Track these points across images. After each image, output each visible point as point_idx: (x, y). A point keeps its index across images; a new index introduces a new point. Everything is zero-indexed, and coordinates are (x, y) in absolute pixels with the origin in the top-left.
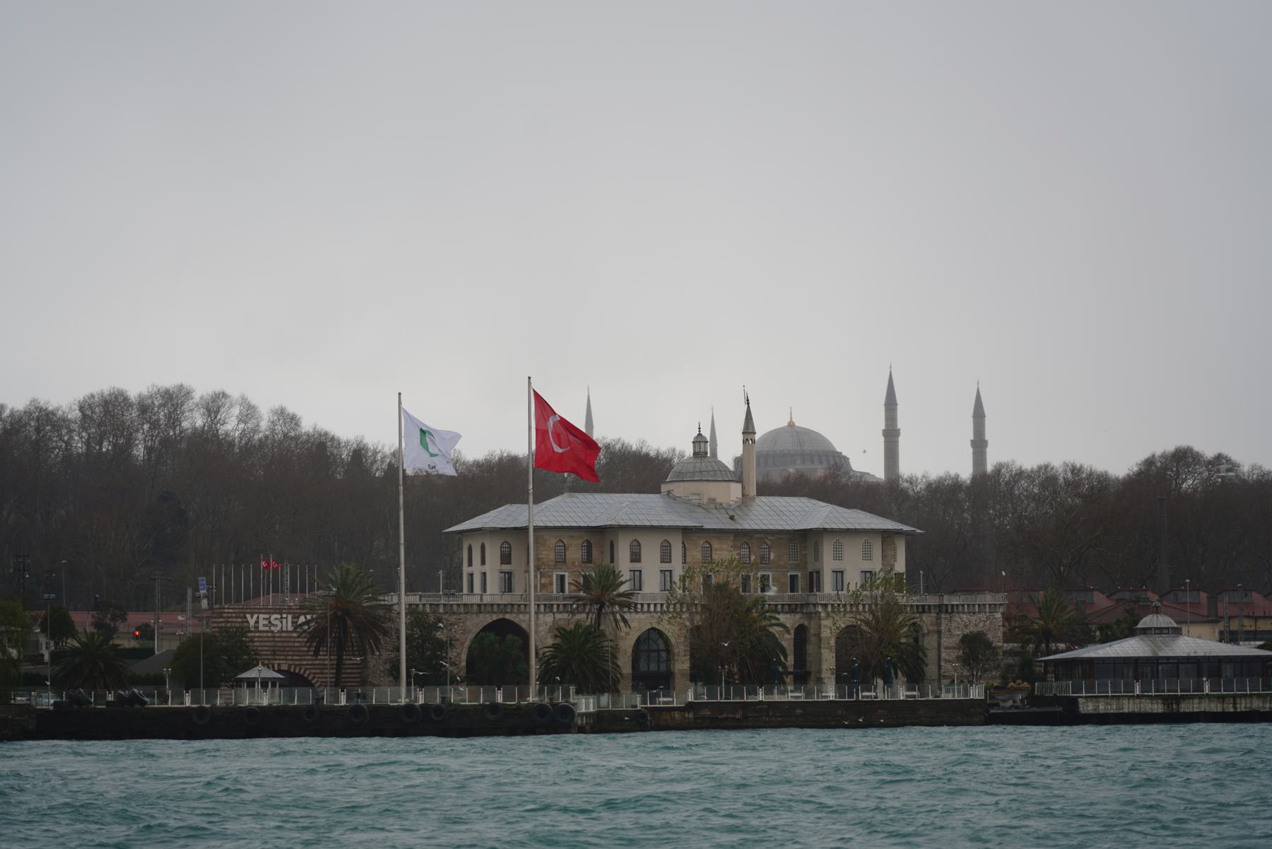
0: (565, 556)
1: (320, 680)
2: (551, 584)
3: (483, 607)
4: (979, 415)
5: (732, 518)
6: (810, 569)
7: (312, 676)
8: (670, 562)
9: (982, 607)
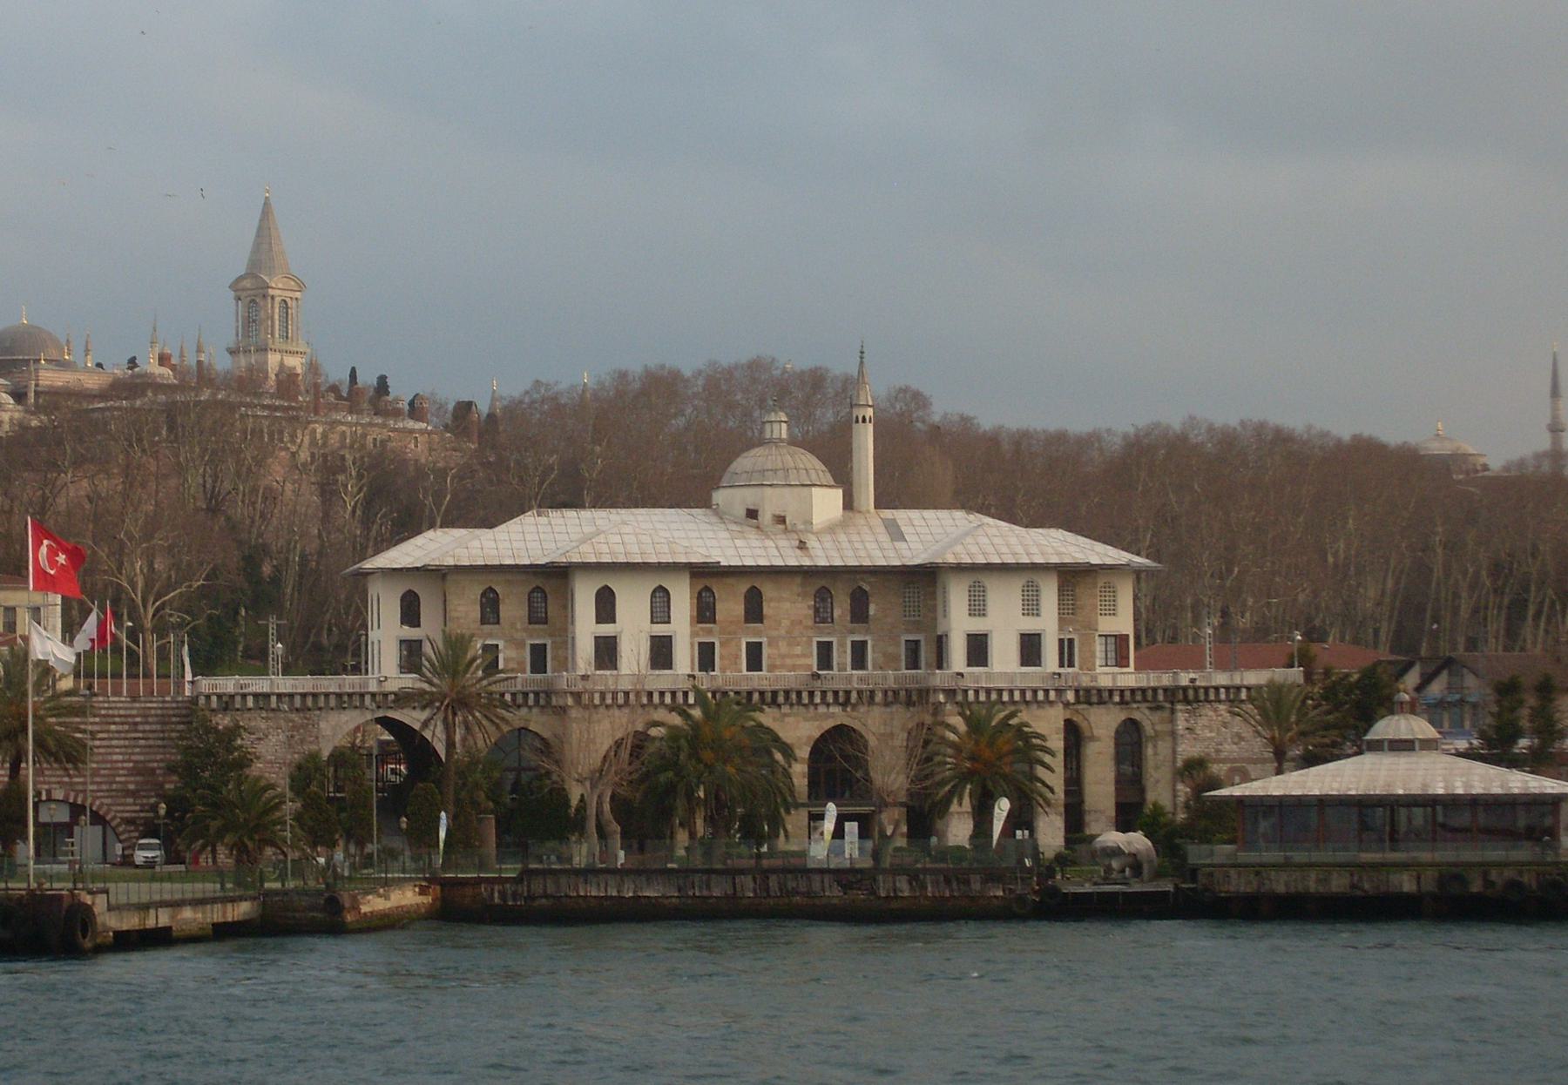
0: (546, 613)
1: (119, 815)
4: (1555, 364)
7: (105, 808)
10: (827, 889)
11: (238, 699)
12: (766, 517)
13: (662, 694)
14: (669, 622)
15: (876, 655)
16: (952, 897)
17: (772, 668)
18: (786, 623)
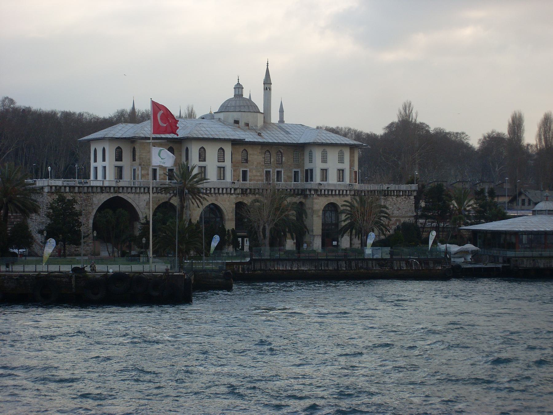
2: (148, 174)
3: (104, 189)
4: (268, 64)
5: (259, 134)
6: (306, 168)
8: (205, 161)
9: (404, 192)
10: (374, 267)
11: (63, 188)
12: (242, 124)
13: (223, 189)
14: (224, 162)
15: (285, 176)
16: (422, 269)
17: (250, 180)
18: (255, 163)
